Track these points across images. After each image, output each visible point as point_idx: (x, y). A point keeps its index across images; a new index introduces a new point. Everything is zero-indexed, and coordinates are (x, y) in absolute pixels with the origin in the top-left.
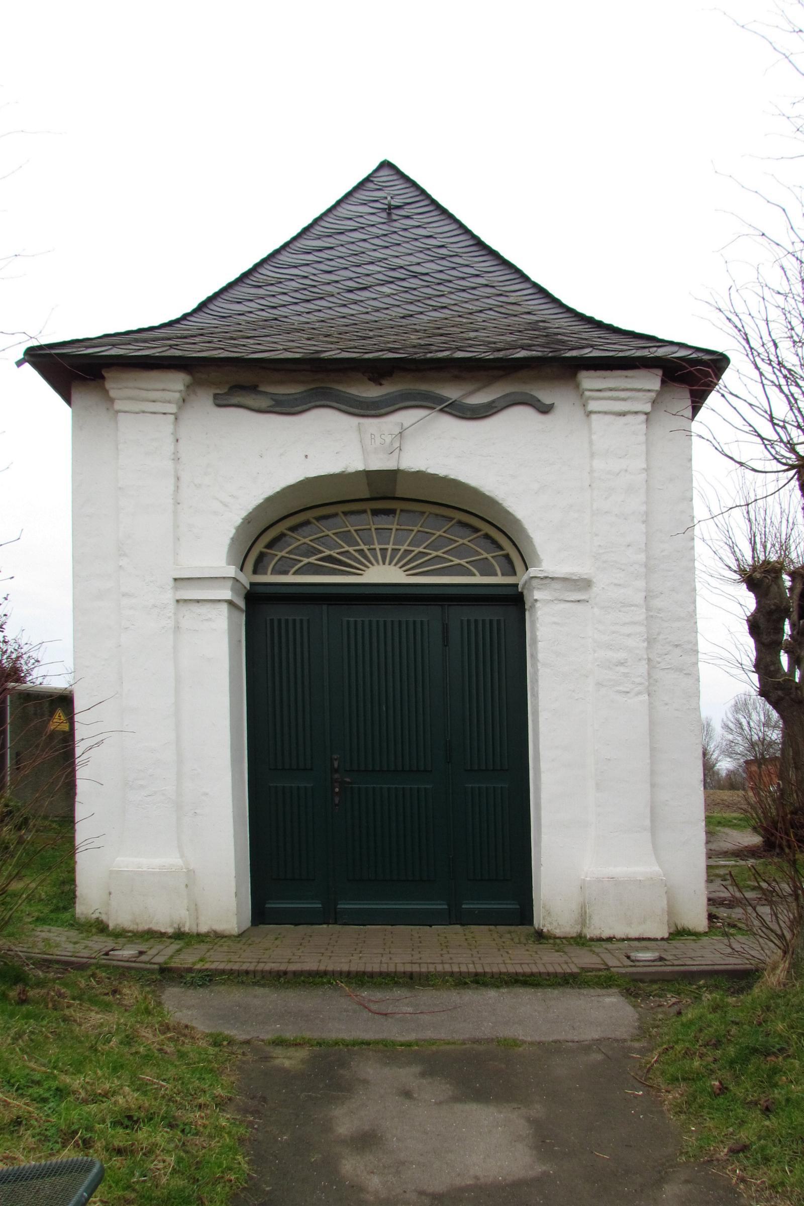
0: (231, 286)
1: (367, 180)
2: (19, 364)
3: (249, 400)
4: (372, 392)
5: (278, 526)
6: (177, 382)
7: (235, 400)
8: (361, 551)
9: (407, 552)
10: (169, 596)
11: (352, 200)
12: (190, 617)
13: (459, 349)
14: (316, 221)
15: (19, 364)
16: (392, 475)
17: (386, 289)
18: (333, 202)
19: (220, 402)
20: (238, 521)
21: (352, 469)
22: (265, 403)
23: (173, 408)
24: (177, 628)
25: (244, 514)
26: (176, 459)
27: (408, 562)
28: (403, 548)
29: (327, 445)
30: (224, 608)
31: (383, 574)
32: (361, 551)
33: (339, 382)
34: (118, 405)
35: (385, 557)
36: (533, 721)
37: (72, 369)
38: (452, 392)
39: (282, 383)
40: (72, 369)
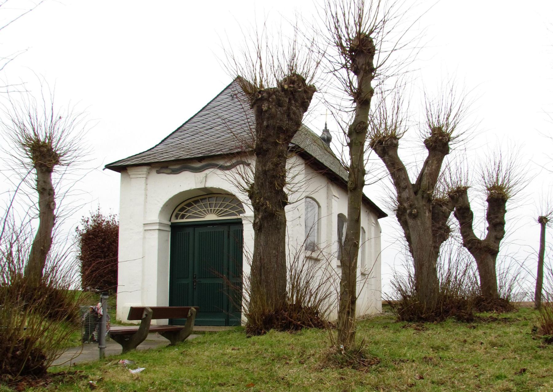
0: (173, 133)
1: (231, 85)
2: (104, 169)
3: (165, 171)
4: (198, 165)
5: (183, 203)
6: (145, 169)
7: (162, 171)
8: (195, 213)
9: (218, 210)
10: (142, 229)
11: (224, 93)
12: (148, 234)
13: (218, 151)
14: (208, 104)
15: (104, 169)
16: (205, 189)
17: (218, 128)
18: (216, 96)
19: (158, 172)
20: (162, 206)
21: (193, 188)
22: (169, 171)
23: (145, 176)
24: (144, 238)
25: (163, 204)
26: (146, 189)
27: (219, 213)
28: (217, 209)
29: (187, 182)
30: (157, 232)
31: (211, 217)
32: (195, 213)
33: (190, 163)
34: (131, 176)
35: (211, 212)
36: (362, 252)
37: (120, 167)
38: (221, 163)
39: (175, 165)
40: (120, 167)
